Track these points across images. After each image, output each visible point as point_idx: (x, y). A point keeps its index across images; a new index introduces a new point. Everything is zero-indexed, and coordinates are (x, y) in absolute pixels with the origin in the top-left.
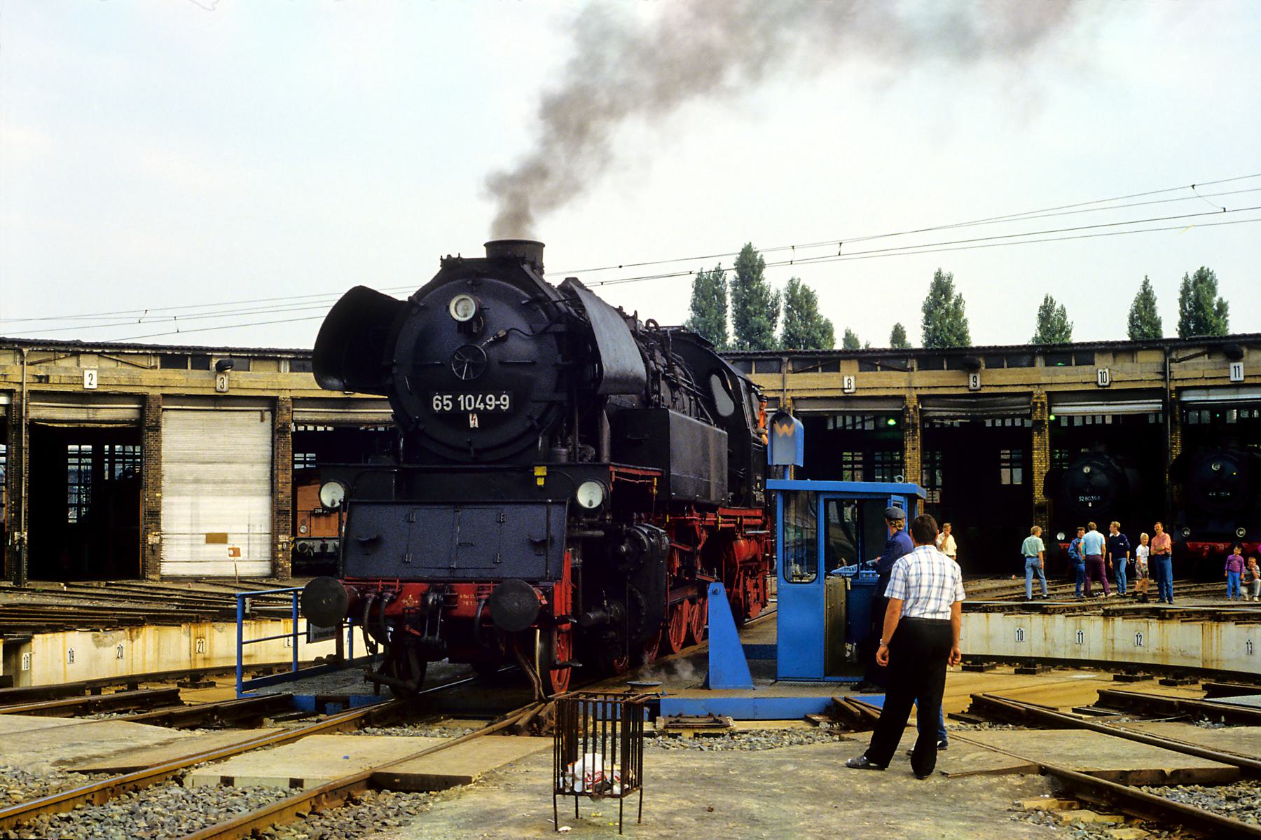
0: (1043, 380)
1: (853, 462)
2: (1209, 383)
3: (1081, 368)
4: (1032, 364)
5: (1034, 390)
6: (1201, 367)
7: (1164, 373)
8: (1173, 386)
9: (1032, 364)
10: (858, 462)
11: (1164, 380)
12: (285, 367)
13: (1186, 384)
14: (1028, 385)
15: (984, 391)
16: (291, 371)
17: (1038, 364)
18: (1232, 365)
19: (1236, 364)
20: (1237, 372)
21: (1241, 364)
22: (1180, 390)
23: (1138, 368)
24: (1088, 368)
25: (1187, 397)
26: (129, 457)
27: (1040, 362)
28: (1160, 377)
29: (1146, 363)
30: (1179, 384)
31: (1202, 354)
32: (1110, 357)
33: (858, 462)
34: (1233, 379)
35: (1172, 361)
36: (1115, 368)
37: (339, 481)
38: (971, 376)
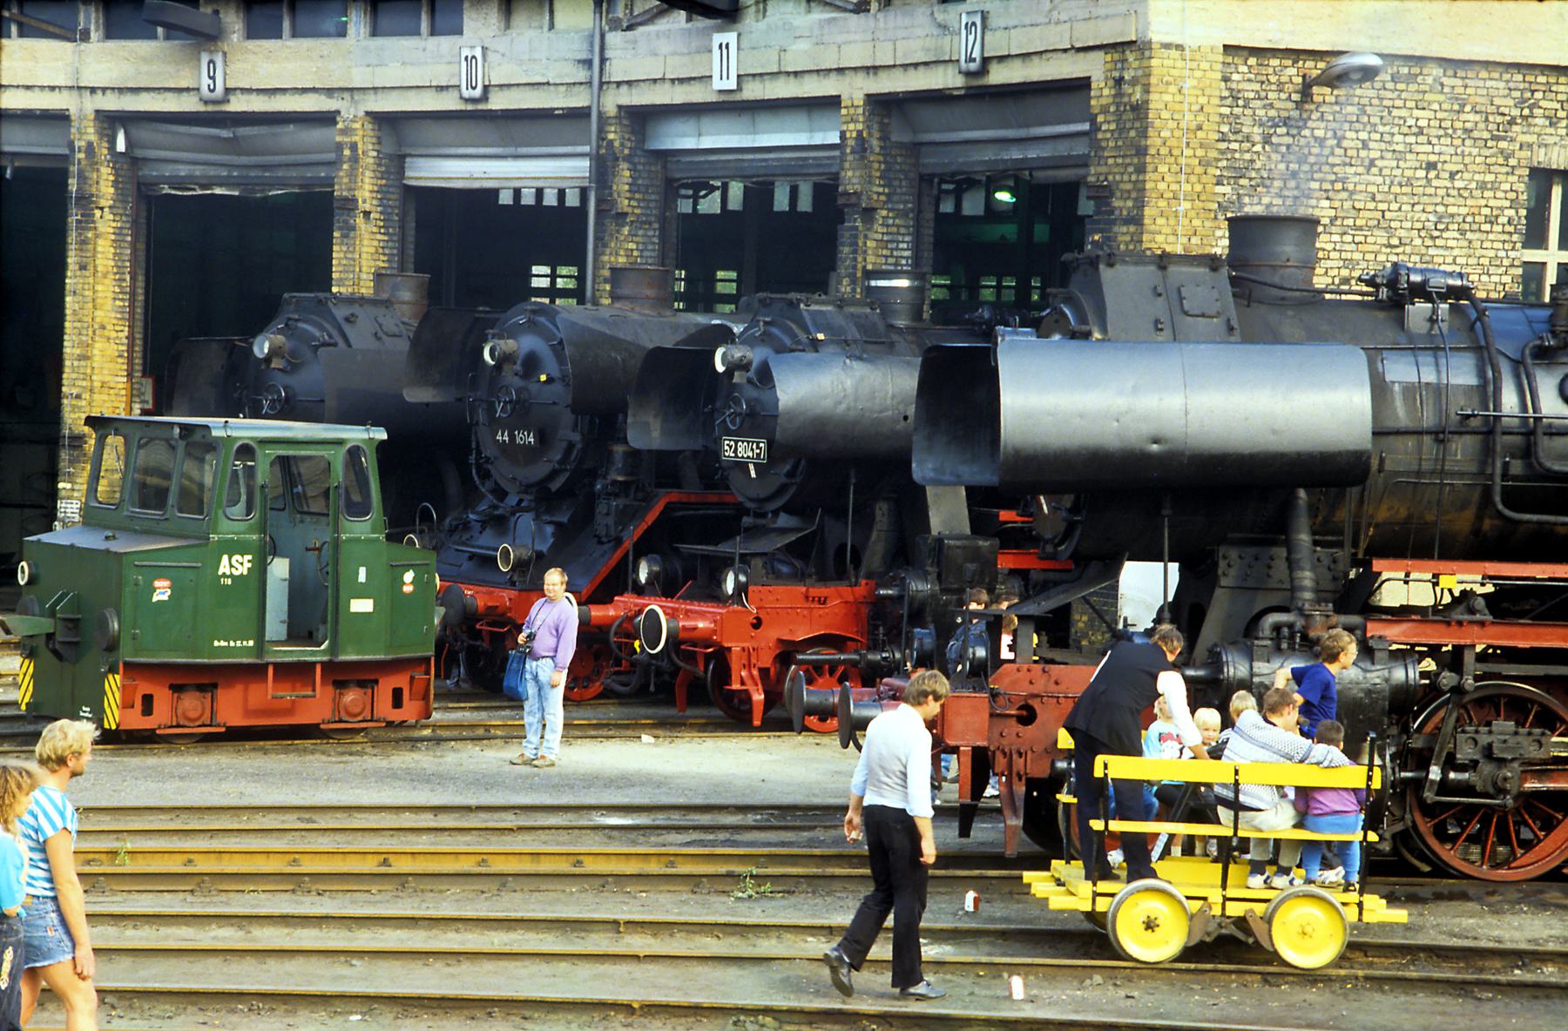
4: (342, 33)
8: (612, 101)
9: (342, 33)
14: (330, 92)
17: (351, 29)
18: (718, 38)
21: (730, 37)
25: (683, 138)
28: (582, 75)
34: (717, 84)
38: (205, 58)
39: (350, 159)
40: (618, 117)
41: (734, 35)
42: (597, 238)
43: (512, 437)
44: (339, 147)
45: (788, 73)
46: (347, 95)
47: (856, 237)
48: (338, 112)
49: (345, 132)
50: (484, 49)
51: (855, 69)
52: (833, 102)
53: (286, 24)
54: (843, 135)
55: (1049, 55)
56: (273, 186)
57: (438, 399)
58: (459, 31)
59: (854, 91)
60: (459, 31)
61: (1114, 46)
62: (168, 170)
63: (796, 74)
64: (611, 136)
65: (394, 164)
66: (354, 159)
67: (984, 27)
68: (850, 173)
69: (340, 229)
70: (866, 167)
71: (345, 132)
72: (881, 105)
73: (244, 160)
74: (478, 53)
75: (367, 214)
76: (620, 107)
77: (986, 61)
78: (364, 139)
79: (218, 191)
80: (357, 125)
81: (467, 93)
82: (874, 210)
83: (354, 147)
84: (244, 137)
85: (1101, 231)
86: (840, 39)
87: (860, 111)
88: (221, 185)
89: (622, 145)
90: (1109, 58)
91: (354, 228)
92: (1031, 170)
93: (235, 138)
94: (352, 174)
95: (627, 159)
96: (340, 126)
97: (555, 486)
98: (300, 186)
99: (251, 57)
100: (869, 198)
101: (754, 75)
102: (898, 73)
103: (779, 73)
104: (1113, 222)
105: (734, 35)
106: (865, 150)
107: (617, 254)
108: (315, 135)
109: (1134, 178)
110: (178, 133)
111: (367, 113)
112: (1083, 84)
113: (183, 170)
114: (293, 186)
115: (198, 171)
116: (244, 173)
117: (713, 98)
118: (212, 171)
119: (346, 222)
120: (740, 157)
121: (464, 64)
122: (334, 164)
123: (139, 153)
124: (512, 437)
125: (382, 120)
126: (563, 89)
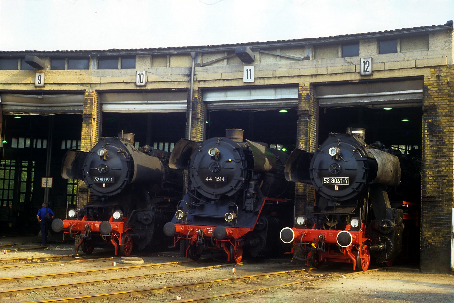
0: (94, 80)
1: (10, 166)
2: (226, 84)
3: (124, 71)
4: (87, 68)
5: (87, 89)
6: (220, 71)
7: (190, 76)
8: (196, 87)
9: (87, 68)
10: (13, 166)
11: (189, 81)
12: (93, 65)
13: (207, 85)
14: (82, 84)
15: (47, 88)
16: (98, 68)
17: (91, 67)
18: (245, 68)
19: (249, 67)
20: (249, 74)
21: (252, 67)
22: (204, 91)
23: (168, 71)
24: (129, 71)
25: (211, 97)
26: (8, 166)
27: (93, 65)
28: (186, 79)
29: (177, 67)
30: (202, 85)
31: (223, 60)
32: (148, 62)
33: (13, 166)
34: (245, 80)
35: (197, 65)
36: (152, 70)
37: (303, 217)
38: (37, 75)
39: (90, 103)
40: (198, 91)
41: (253, 67)
42: (192, 126)
43: (214, 179)
44: (86, 100)
45: (276, 77)
46: (88, 85)
47: (308, 123)
48: (85, 90)
49: (88, 96)
50: (146, 72)
51: (306, 76)
52: (296, 86)
53: (66, 66)
54: (300, 95)
55: (402, 70)
56: (51, 112)
57: (176, 168)
58: (134, 67)
59: (306, 82)
60: (134, 67)
61: (435, 67)
62: (14, 108)
63: (279, 77)
64: (196, 96)
65: (100, 105)
66: (92, 103)
67: (372, 63)
68: (304, 105)
69: (85, 123)
70: (310, 104)
71: (88, 96)
72: (314, 86)
73: (43, 105)
74: (144, 73)
75: (94, 119)
76: (199, 88)
77: (373, 71)
78: (95, 97)
79: (31, 114)
80: (94, 94)
81: (138, 84)
82: (311, 116)
83: (92, 100)
84: (46, 98)
85: (432, 119)
86: (300, 67)
87: (309, 87)
88: (32, 112)
89: (199, 99)
90: (433, 70)
91: (91, 123)
92: (372, 105)
93: (42, 99)
94: (91, 108)
95: (200, 103)
96: (87, 94)
97: (229, 195)
98: (62, 113)
99: (54, 74)
100: (311, 112)
101: (260, 78)
102: (221, 81)
103: (273, 77)
104: (439, 116)
105: (253, 67)
106: (309, 99)
107: (197, 130)
108: (80, 97)
109: (448, 103)
110: (22, 97)
111: (96, 90)
112: (421, 78)
113: (19, 108)
114: (59, 112)
115: (25, 108)
116: (42, 109)
117: (242, 85)
118: (30, 108)
119: (88, 121)
120: (245, 103)
121: (138, 76)
122: (86, 104)
123: (4, 103)
124: (214, 179)
125: (100, 93)
126: (176, 83)
